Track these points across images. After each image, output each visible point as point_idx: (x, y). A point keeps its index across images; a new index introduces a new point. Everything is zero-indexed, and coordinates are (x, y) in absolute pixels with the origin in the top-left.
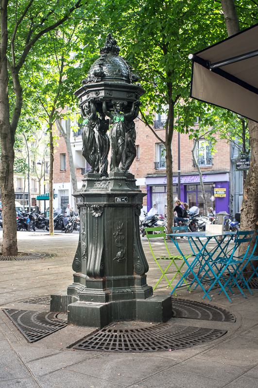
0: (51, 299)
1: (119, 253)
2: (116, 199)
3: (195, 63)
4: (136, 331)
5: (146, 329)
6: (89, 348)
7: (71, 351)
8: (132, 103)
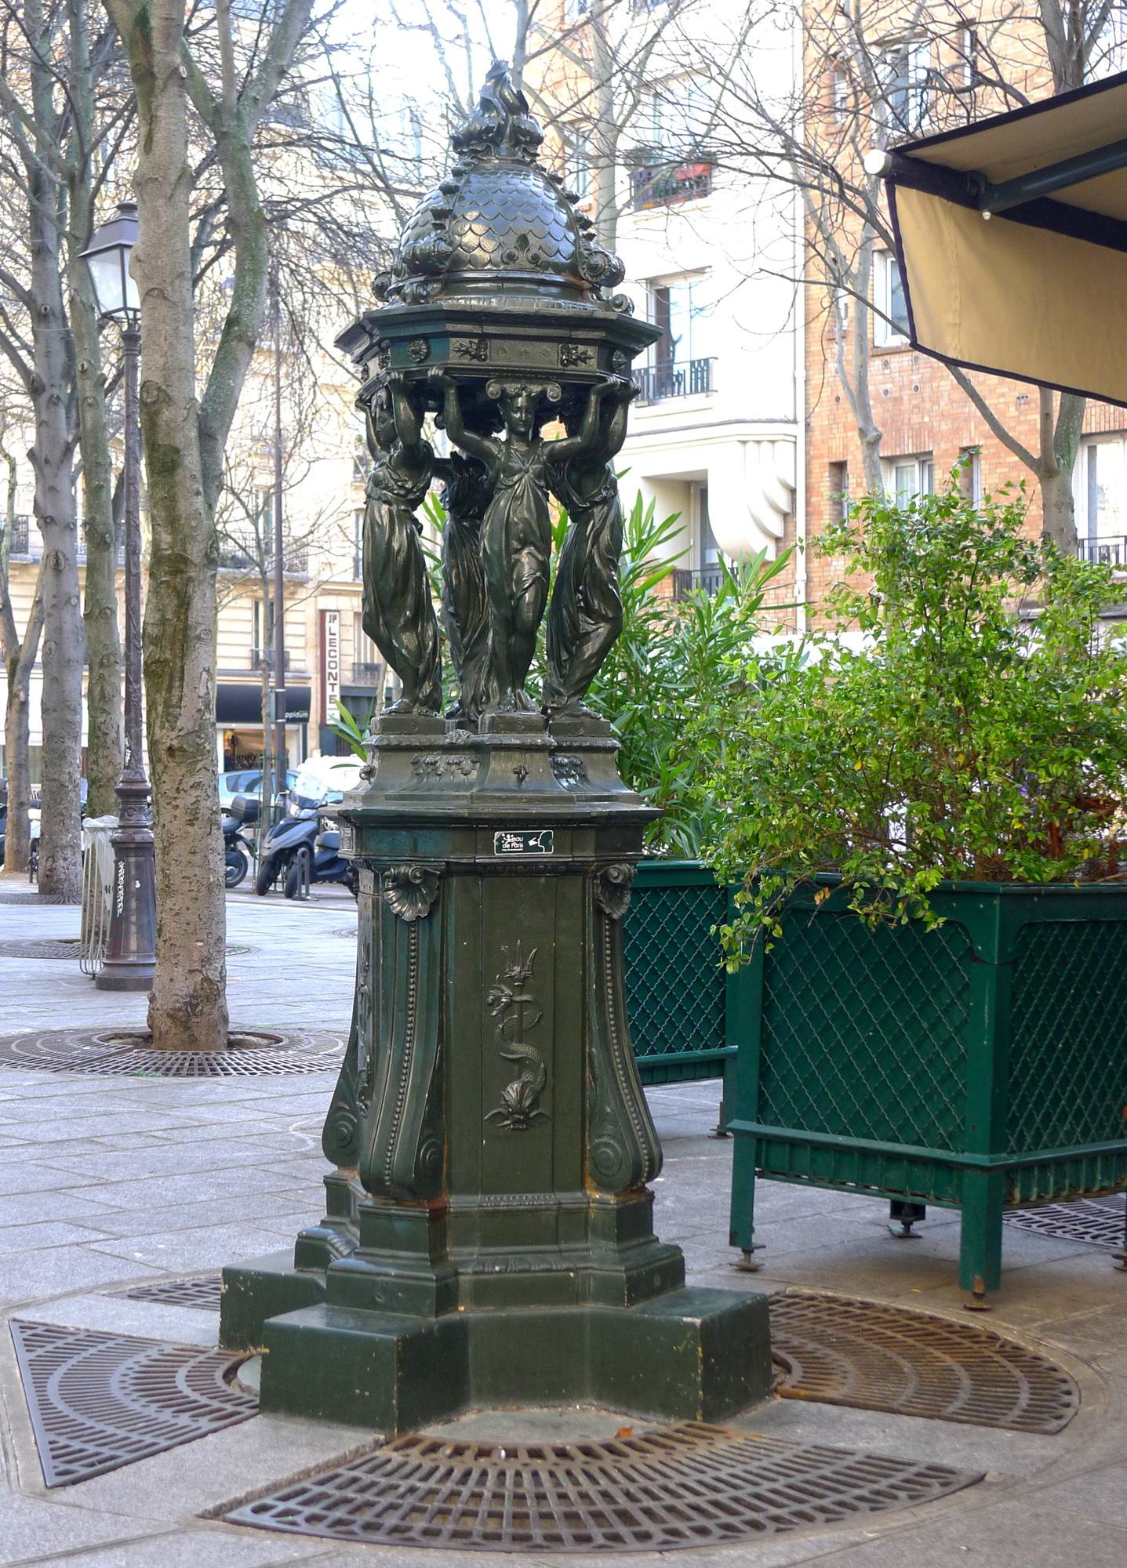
0: (224, 1288)
1: (512, 1091)
2: (501, 838)
3: (901, 192)
4: (605, 1453)
5: (647, 1440)
6: (294, 1523)
7: (217, 1540)
8: (587, 389)
